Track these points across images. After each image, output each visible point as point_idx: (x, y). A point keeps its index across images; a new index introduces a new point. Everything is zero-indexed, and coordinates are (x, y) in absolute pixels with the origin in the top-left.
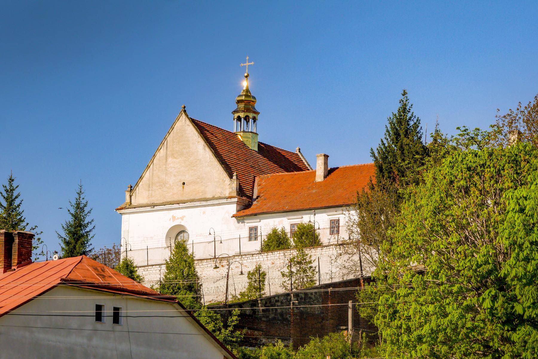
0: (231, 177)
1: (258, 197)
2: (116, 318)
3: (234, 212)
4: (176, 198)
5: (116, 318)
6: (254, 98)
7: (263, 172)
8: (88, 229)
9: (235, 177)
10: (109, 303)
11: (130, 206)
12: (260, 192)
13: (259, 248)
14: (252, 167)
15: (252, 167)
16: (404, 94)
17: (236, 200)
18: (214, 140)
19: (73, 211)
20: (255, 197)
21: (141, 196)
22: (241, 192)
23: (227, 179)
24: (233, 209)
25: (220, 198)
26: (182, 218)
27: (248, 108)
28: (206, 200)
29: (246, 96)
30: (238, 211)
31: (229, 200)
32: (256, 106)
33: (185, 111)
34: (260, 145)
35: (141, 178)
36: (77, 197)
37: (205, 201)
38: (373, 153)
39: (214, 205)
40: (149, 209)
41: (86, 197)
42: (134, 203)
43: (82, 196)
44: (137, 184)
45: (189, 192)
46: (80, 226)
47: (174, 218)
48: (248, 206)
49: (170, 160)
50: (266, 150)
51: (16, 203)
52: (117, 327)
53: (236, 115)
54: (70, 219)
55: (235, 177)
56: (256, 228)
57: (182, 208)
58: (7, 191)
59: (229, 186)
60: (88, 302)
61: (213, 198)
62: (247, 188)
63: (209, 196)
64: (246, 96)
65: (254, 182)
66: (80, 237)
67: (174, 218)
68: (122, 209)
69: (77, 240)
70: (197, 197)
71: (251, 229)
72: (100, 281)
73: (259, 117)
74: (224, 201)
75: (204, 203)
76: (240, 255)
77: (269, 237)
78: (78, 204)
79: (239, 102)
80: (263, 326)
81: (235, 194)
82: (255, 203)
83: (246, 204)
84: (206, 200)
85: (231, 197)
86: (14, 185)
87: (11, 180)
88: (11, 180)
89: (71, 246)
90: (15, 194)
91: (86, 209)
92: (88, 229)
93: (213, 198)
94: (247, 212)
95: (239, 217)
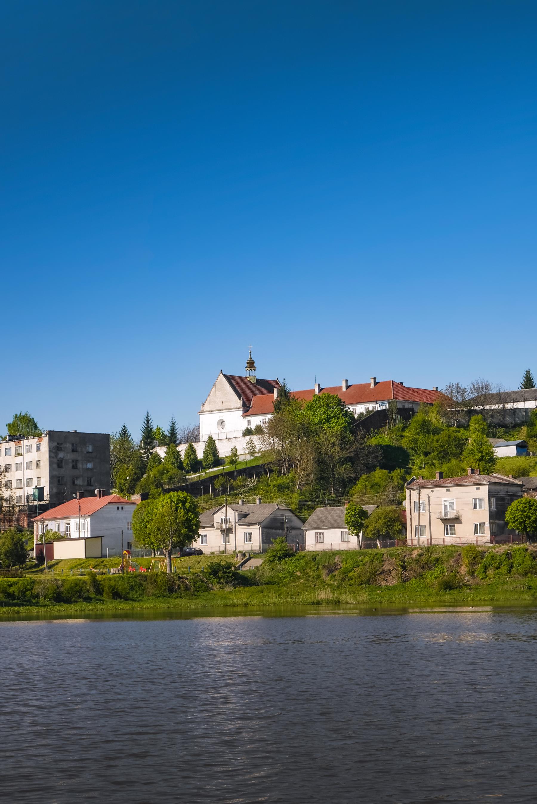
2: (122, 508)
3: (242, 414)
4: (220, 408)
5: (122, 508)
10: (120, 506)
11: (203, 411)
18: (234, 383)
21: (206, 408)
22: (244, 405)
24: (241, 413)
25: (237, 408)
26: (223, 416)
29: (250, 361)
34: (257, 380)
45: (225, 406)
49: (217, 392)
50: (260, 382)
54: (170, 428)
56: (250, 421)
59: (239, 403)
60: (115, 507)
61: (234, 408)
62: (248, 402)
71: (248, 421)
72: (118, 501)
79: (247, 363)
83: (247, 410)
84: (231, 409)
86: (149, 414)
90: (149, 418)
91: (176, 424)
93: (234, 408)
94: (247, 414)
95: (244, 416)
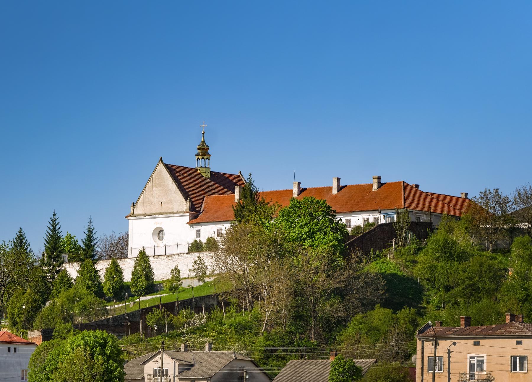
0: (186, 201)
1: (203, 211)
2: (15, 350)
3: (188, 221)
5: (15, 350)
6: (207, 146)
7: (210, 193)
8: (95, 242)
9: (188, 201)
10: (12, 347)
11: (133, 215)
12: (204, 208)
13: (187, 250)
14: (204, 190)
15: (204, 190)
16: (250, 175)
17: (189, 214)
18: (179, 177)
19: (87, 233)
20: (201, 211)
21: (139, 210)
23: (185, 201)
24: (187, 219)
26: (161, 223)
27: (204, 151)
28: (173, 213)
30: (190, 220)
31: (185, 214)
32: (209, 152)
33: (162, 161)
34: (212, 173)
35: (139, 199)
36: (89, 224)
37: (172, 213)
38: (233, 207)
39: (177, 216)
40: (143, 217)
41: (94, 225)
42: (135, 213)
43: (91, 224)
44: (137, 202)
46: (91, 240)
47: (156, 223)
48: (196, 217)
49: (154, 189)
51: (57, 227)
52: (15, 354)
53: (197, 157)
54: (85, 237)
55: (188, 201)
57: (161, 217)
58: (52, 221)
59: (185, 206)
61: (177, 213)
62: (197, 205)
63: (175, 211)
64: (203, 145)
65: (203, 200)
66: (90, 247)
67: (156, 223)
68: (128, 217)
69: (89, 249)
70: (169, 211)
72: (10, 340)
73: (211, 158)
74: (183, 214)
75: (172, 215)
76: (178, 254)
77: (192, 244)
78: (89, 229)
79: (199, 149)
80: (112, 328)
81: (188, 211)
82: (201, 215)
83: (196, 215)
84: (173, 213)
85: (186, 212)
86: (56, 217)
87: (55, 215)
88: (55, 215)
89: (85, 252)
90: (57, 222)
91: (94, 231)
92: (95, 242)
93: (177, 213)
